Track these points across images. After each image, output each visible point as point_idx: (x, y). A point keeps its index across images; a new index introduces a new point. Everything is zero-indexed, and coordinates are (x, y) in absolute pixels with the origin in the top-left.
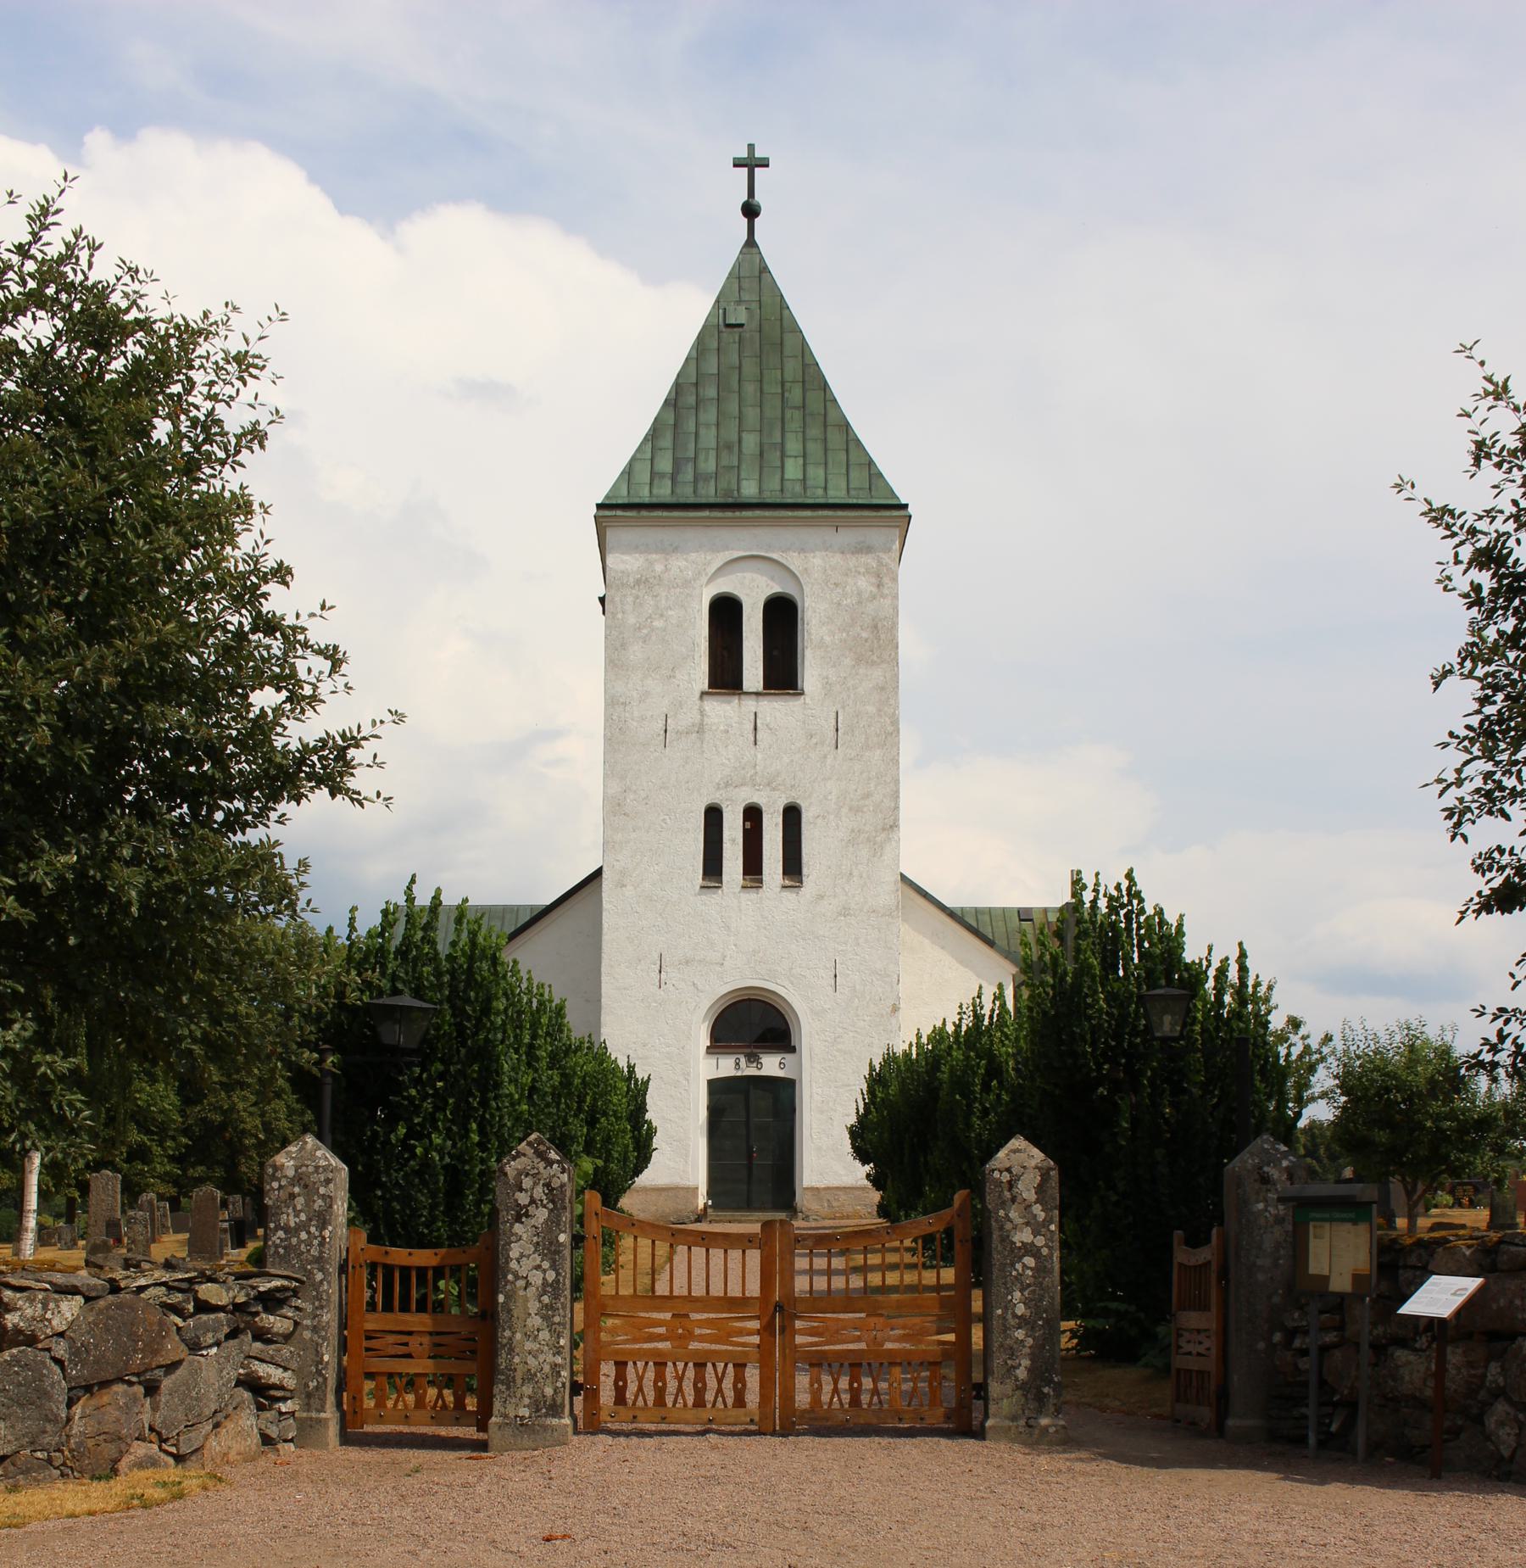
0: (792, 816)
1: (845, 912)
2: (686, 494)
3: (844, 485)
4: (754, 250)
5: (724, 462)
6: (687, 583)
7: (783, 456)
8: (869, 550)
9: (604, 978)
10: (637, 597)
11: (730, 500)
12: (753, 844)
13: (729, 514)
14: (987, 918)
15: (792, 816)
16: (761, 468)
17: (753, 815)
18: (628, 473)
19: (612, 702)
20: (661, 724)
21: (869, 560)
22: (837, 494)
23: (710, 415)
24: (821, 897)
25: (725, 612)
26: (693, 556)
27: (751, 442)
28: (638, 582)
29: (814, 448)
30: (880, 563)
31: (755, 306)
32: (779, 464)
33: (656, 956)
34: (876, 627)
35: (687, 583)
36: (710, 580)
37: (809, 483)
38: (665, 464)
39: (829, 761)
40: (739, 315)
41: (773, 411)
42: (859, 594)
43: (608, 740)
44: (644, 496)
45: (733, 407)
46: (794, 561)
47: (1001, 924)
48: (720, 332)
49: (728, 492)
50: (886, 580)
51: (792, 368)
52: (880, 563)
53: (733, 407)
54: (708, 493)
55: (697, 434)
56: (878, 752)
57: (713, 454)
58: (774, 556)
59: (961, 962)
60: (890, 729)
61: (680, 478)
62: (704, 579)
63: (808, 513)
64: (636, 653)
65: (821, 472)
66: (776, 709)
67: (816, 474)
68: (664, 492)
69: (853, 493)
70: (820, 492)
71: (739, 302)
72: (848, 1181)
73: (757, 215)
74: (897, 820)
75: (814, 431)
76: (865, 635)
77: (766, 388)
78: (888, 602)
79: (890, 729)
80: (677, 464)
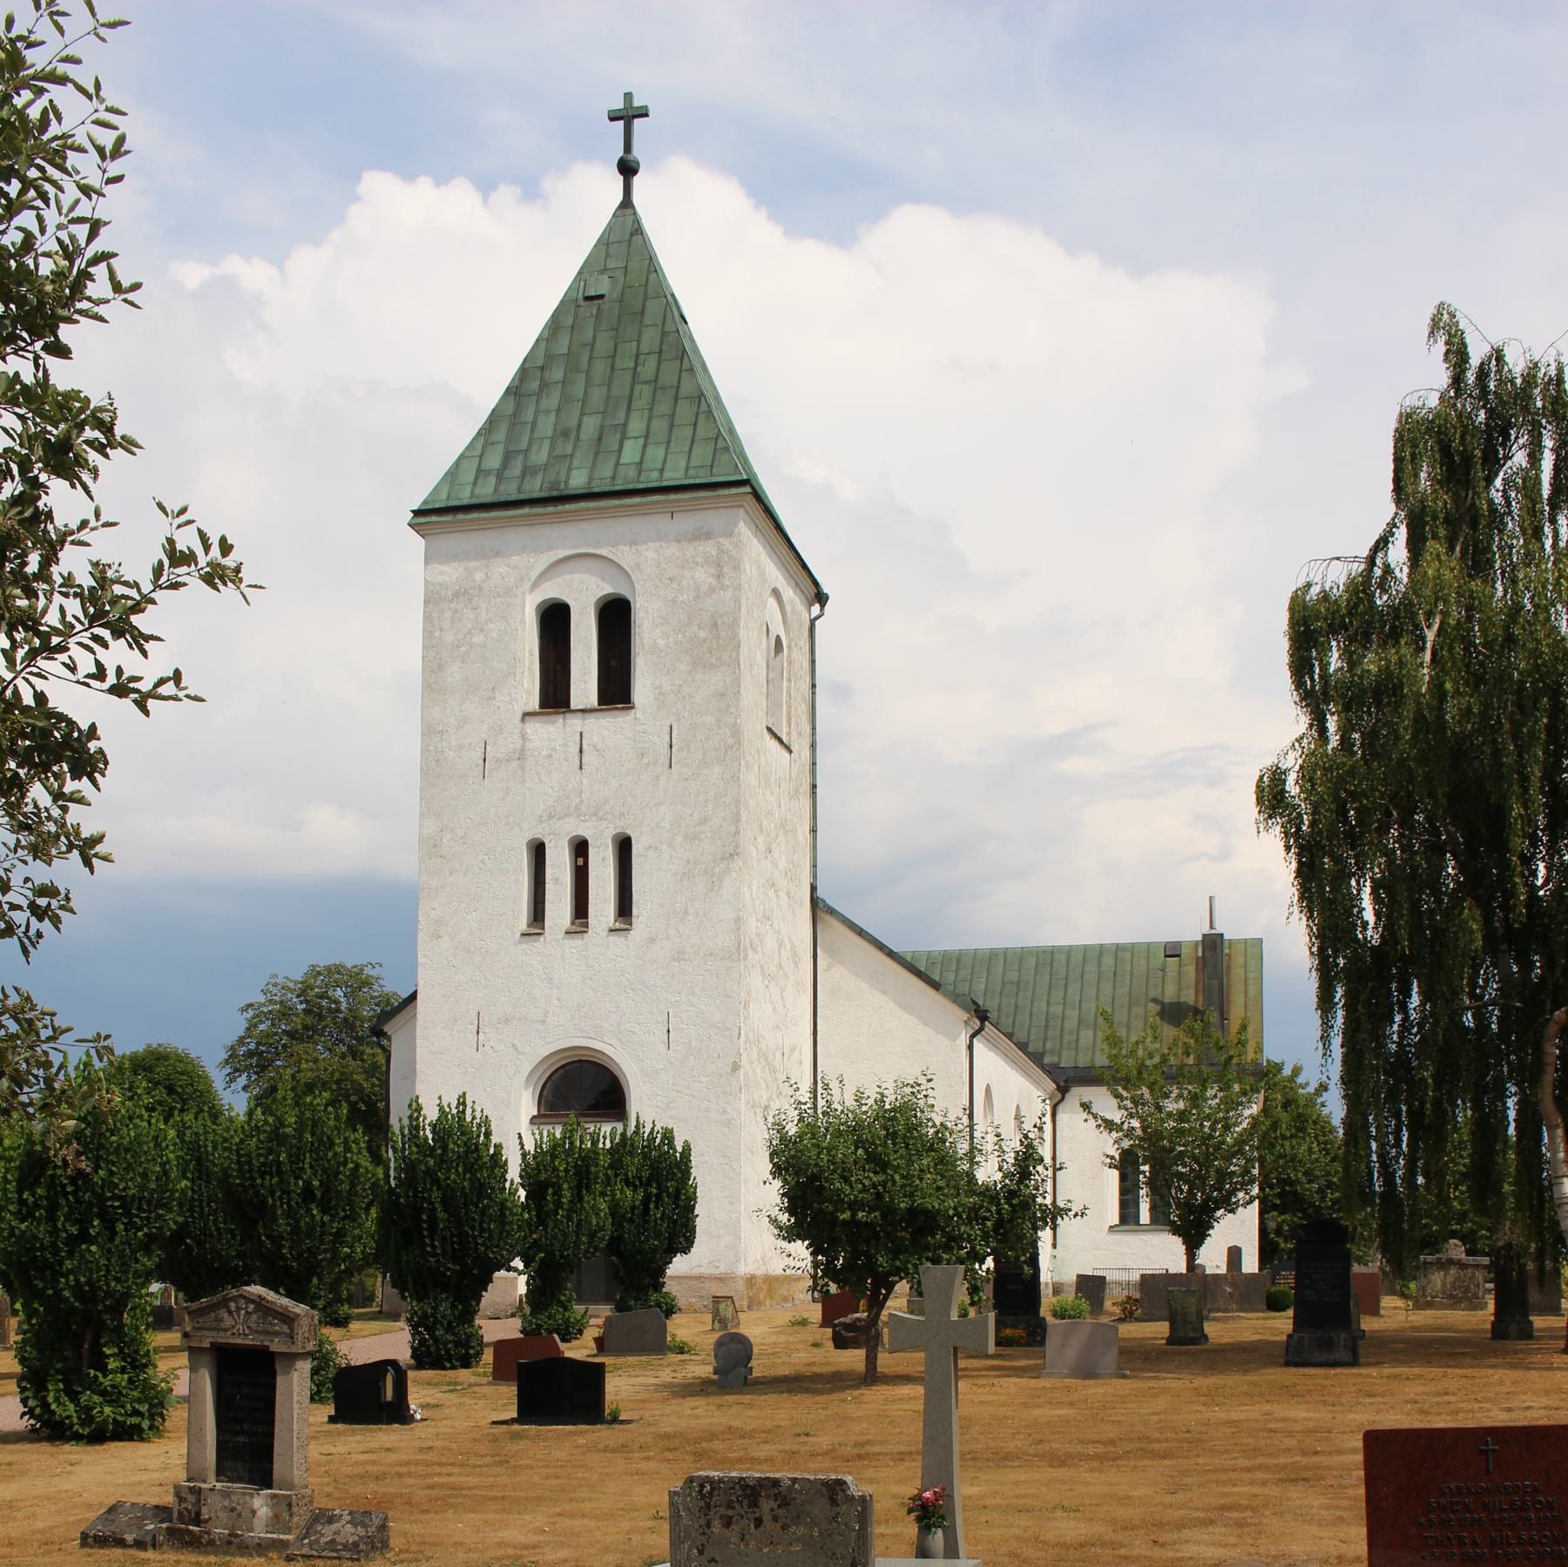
0: (624, 847)
1: (679, 956)
2: (510, 491)
3: (683, 464)
4: (629, 211)
5: (558, 452)
6: (509, 591)
7: (624, 437)
8: (707, 536)
9: (419, 1042)
10: (456, 611)
11: (555, 493)
12: (586, 881)
13: (551, 509)
14: (1128, 955)
15: (624, 847)
16: (597, 453)
17: (581, 848)
18: (452, 475)
19: (430, 731)
20: (480, 754)
21: (708, 548)
22: (674, 476)
23: (552, 400)
24: (652, 940)
25: (555, 619)
26: (515, 560)
27: (590, 426)
28: (457, 595)
29: (660, 426)
30: (721, 551)
31: (619, 273)
32: (616, 447)
33: (474, 1016)
34: (715, 624)
35: (509, 591)
36: (536, 585)
37: (645, 466)
38: (494, 461)
39: (662, 783)
40: (602, 286)
41: (621, 387)
42: (697, 588)
43: (425, 773)
44: (465, 497)
45: (578, 390)
46: (624, 555)
47: (1143, 961)
48: (582, 304)
49: (554, 485)
50: (726, 569)
51: (650, 337)
52: (721, 551)
53: (578, 390)
54: (535, 487)
55: (534, 424)
56: (717, 769)
57: (547, 442)
58: (603, 552)
59: (905, 1008)
60: (731, 741)
61: (508, 473)
62: (527, 585)
63: (637, 500)
64: (454, 674)
65: (661, 452)
66: (608, 729)
67: (656, 454)
68: (486, 492)
69: (691, 472)
70: (655, 475)
71: (604, 271)
72: (776, 1266)
73: (635, 172)
74: (737, 847)
75: (663, 407)
76: (702, 634)
77: (618, 365)
78: (728, 594)
79: (731, 741)
80: (507, 458)
